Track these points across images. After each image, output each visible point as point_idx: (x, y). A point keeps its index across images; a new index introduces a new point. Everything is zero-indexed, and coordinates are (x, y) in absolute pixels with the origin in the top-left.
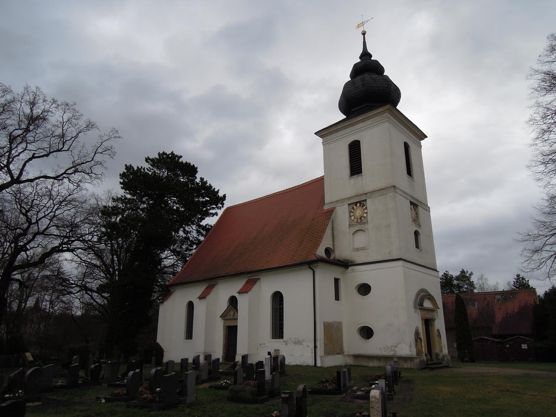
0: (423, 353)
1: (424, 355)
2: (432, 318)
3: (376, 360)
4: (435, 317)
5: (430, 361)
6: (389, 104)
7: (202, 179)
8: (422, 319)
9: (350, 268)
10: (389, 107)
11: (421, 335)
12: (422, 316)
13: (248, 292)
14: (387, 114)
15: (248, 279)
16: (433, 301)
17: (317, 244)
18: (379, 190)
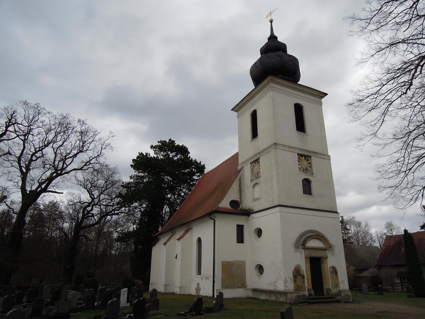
0: (305, 289)
1: (307, 290)
2: (323, 256)
3: (264, 294)
4: (327, 255)
5: (314, 296)
6: (269, 76)
7: (190, 156)
8: (305, 258)
9: (251, 215)
10: (270, 78)
11: (304, 272)
12: (306, 255)
13: (181, 239)
14: (271, 84)
15: (187, 228)
16: (324, 241)
17: (222, 197)
18: (267, 148)
